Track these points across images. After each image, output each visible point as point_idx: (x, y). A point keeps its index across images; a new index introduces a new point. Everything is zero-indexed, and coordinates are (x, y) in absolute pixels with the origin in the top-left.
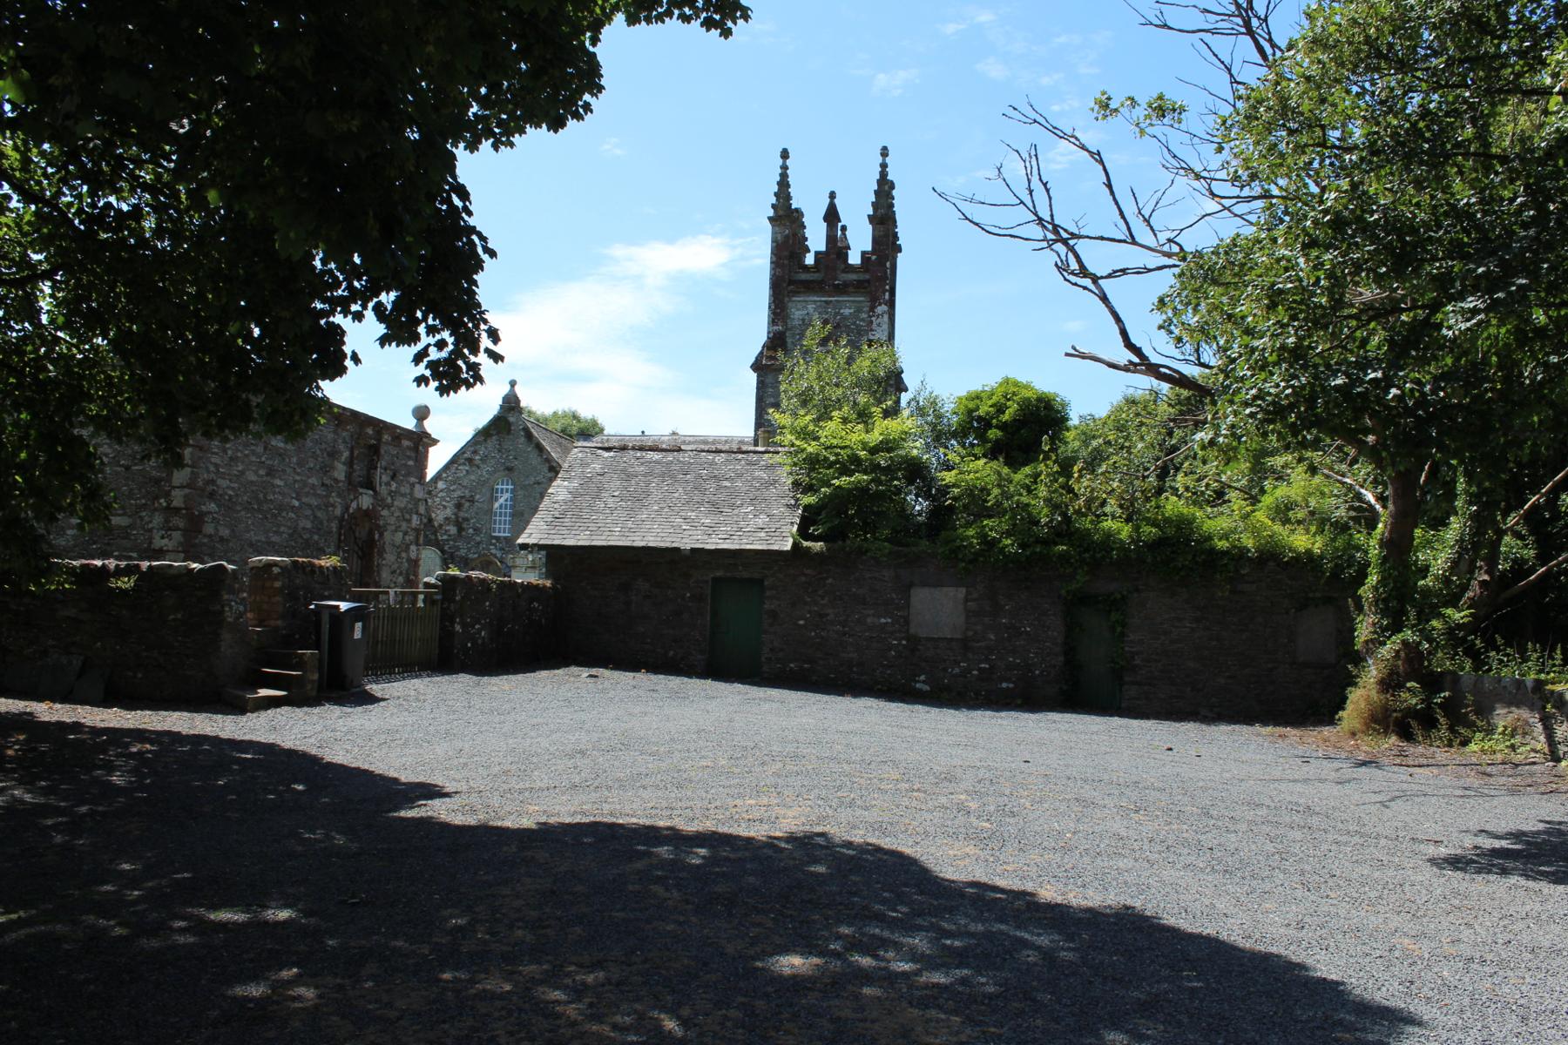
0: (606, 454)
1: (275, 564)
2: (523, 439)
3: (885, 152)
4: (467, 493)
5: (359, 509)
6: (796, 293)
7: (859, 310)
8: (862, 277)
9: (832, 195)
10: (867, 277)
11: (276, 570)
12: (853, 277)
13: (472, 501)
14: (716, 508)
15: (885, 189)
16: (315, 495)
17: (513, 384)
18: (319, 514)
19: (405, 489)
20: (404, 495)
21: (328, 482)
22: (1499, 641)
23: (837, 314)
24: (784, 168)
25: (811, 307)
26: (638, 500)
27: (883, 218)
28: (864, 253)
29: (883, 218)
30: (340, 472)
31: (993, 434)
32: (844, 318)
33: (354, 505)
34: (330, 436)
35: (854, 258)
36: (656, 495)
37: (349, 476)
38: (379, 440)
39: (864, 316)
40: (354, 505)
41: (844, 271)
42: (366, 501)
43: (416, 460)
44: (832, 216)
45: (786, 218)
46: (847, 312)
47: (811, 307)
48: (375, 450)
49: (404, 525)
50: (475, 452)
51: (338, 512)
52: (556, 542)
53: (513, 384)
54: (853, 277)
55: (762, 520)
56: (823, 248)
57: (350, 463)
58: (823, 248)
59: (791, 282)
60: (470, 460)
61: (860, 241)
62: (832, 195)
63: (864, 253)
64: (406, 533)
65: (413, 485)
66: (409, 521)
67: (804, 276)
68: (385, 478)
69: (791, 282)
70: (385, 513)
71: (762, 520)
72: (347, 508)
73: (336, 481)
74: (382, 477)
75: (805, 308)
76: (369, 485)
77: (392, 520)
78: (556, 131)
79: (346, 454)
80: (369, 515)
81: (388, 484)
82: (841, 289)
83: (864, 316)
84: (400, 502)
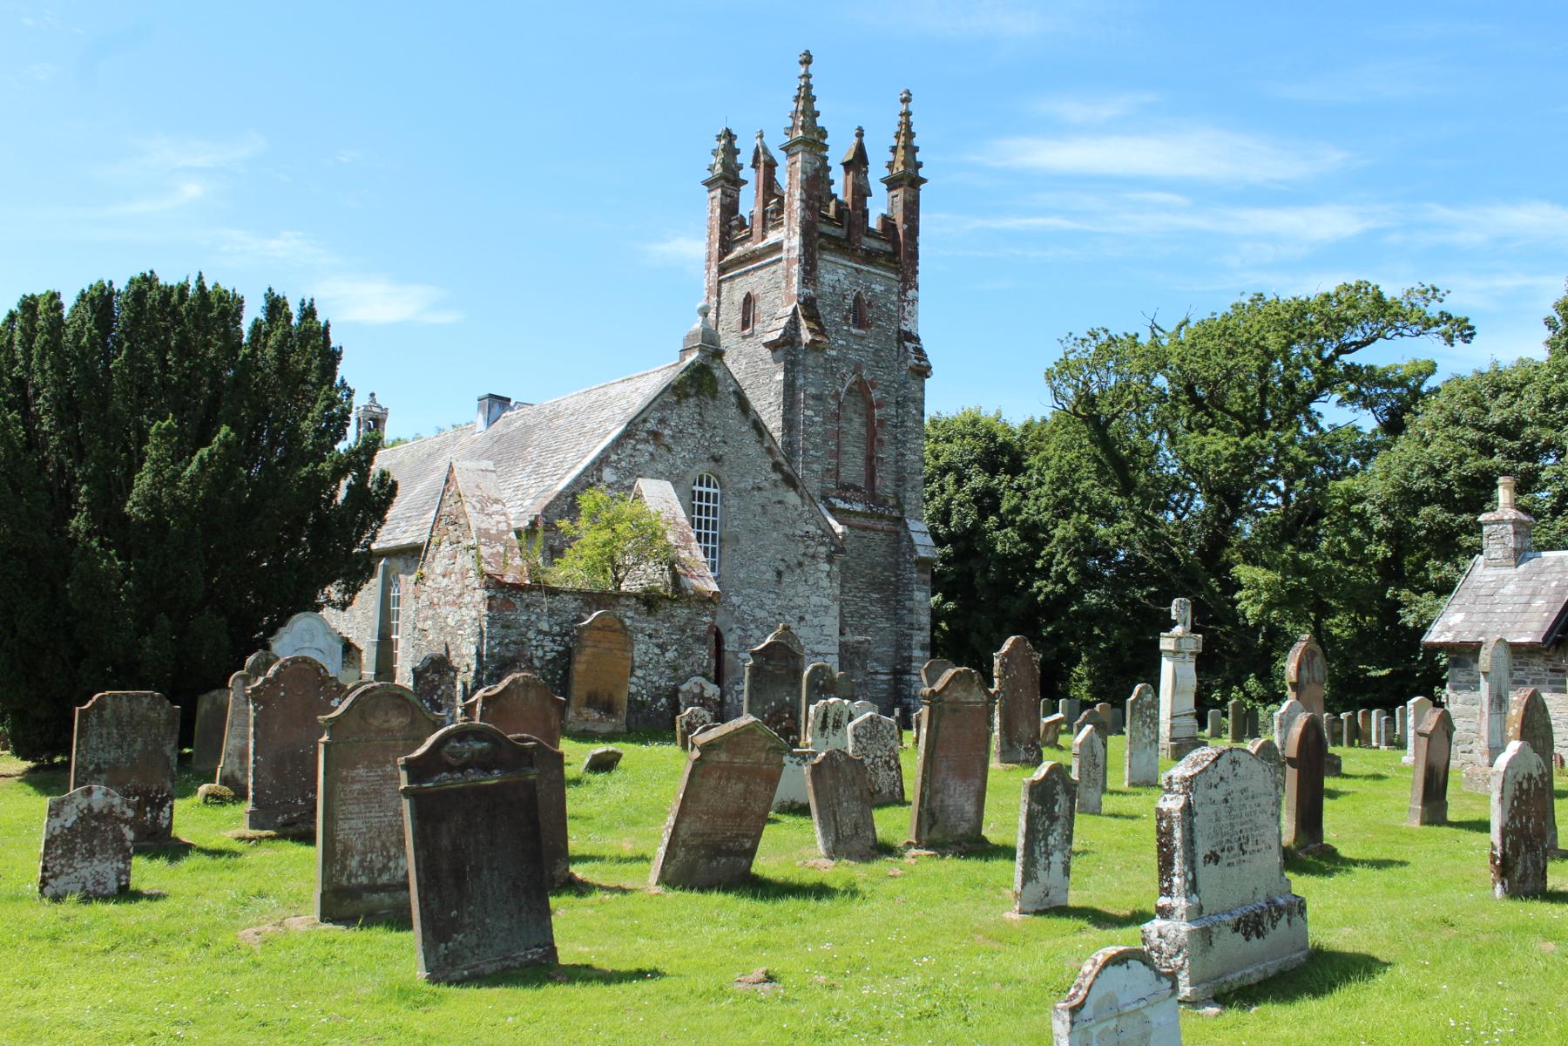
2: (733, 411)
6: (822, 248)
7: (888, 290)
9: (860, 134)
23: (868, 289)
27: (908, 181)
32: (875, 295)
39: (894, 298)
46: (878, 288)
59: (822, 235)
60: (656, 435)
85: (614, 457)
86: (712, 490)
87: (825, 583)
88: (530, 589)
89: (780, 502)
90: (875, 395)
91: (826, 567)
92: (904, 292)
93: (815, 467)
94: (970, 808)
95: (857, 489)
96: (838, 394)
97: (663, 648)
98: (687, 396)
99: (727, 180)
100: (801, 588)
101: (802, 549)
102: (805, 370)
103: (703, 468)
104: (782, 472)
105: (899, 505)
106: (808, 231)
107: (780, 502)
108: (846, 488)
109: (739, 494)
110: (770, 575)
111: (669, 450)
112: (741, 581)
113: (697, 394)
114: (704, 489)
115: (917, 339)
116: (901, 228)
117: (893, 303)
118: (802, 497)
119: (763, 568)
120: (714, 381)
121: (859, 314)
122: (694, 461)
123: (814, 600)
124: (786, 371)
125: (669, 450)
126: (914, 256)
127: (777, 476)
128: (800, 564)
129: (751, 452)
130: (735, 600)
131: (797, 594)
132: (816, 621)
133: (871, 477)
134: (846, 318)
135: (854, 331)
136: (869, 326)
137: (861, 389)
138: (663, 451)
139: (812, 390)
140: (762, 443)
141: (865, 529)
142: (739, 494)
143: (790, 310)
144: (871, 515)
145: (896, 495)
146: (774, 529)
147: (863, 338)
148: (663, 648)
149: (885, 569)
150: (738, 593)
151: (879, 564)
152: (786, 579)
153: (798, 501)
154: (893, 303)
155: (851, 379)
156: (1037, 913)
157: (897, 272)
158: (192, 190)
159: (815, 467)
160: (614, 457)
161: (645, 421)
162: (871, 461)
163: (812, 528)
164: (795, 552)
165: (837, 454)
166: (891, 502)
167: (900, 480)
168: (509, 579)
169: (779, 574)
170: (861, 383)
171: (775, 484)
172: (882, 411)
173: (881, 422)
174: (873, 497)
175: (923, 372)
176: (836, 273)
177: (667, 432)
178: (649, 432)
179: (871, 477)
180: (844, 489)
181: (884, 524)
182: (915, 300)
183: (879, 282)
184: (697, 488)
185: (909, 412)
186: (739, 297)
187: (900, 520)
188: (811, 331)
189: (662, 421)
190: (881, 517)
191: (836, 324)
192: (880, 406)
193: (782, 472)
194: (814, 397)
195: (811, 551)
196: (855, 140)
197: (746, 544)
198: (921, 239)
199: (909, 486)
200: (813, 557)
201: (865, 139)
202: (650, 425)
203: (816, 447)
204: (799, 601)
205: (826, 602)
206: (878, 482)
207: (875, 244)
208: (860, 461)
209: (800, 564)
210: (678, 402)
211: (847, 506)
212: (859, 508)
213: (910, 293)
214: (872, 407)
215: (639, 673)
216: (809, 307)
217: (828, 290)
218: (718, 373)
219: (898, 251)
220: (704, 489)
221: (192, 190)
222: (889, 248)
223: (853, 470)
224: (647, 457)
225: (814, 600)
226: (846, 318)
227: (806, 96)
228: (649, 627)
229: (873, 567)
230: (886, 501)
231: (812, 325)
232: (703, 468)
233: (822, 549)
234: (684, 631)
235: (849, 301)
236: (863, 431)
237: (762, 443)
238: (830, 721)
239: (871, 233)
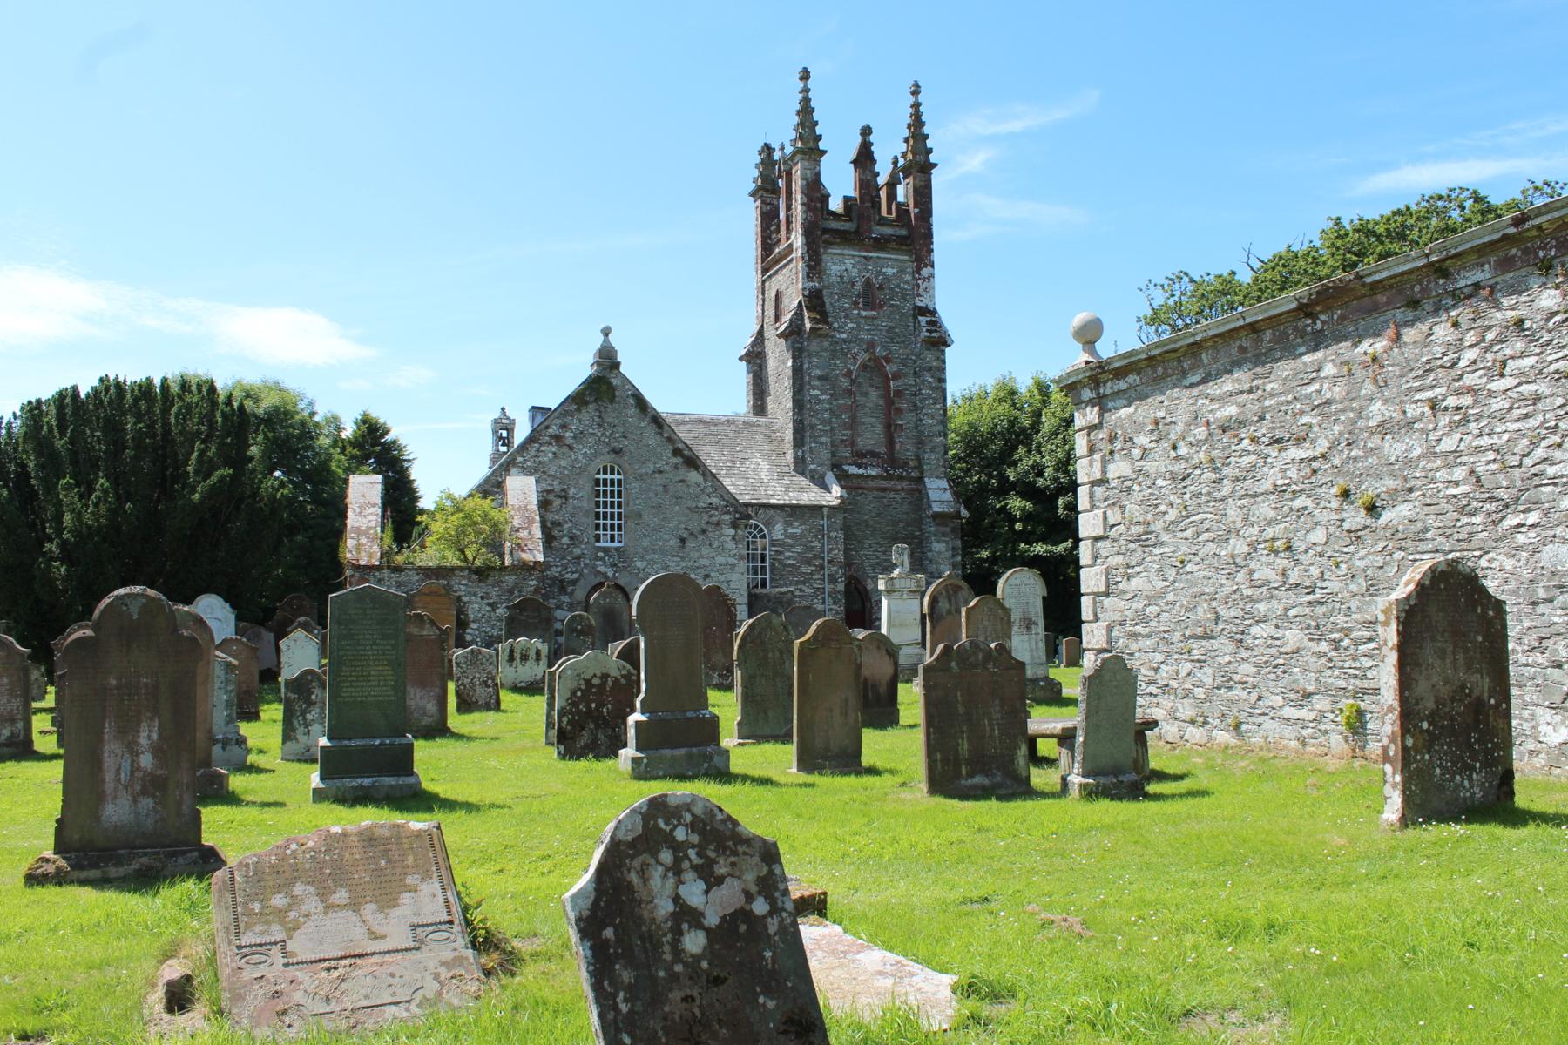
2: (632, 411)
3: (805, 75)
4: (557, 486)
6: (828, 244)
7: (902, 271)
9: (866, 131)
13: (564, 496)
16: (1392, 469)
17: (606, 332)
22: (623, 681)
23: (879, 273)
25: (849, 262)
27: (919, 164)
28: (847, 199)
32: (887, 278)
35: (836, 204)
39: (908, 278)
44: (864, 159)
46: (889, 271)
50: (564, 426)
53: (606, 332)
56: (852, 192)
58: (852, 192)
59: (826, 231)
60: (558, 439)
62: (866, 131)
63: (847, 199)
82: (881, 244)
83: (908, 278)
85: (520, 459)
86: (616, 477)
87: (731, 545)
88: (379, 568)
90: (890, 369)
91: (732, 532)
92: (918, 270)
93: (824, 439)
94: (432, 707)
95: (874, 455)
96: (849, 372)
97: (494, 606)
98: (586, 403)
99: (766, 190)
100: (705, 551)
101: (706, 517)
102: (810, 356)
103: (606, 460)
104: (682, 456)
105: (919, 467)
106: (809, 232)
108: (862, 455)
109: (640, 478)
110: (674, 542)
111: (571, 448)
112: (645, 549)
113: (596, 401)
114: (609, 477)
115: (933, 312)
116: (913, 211)
117: (907, 282)
120: (611, 389)
121: (870, 296)
122: (595, 455)
123: (720, 560)
124: (794, 358)
125: (571, 448)
126: (929, 236)
127: (678, 460)
128: (704, 531)
129: (652, 442)
130: (639, 564)
131: (702, 557)
133: (891, 443)
134: (856, 303)
135: (864, 313)
136: (881, 307)
137: (875, 367)
138: (565, 450)
139: (818, 372)
141: (884, 490)
142: (640, 478)
143: (796, 303)
144: (890, 477)
145: (918, 458)
146: (676, 504)
147: (874, 318)
148: (494, 606)
149: (908, 525)
150: (642, 558)
151: (901, 521)
152: (690, 544)
153: (700, 479)
154: (907, 282)
155: (863, 357)
156: (299, 761)
157: (909, 253)
159: (824, 439)
160: (520, 459)
161: (547, 428)
162: (890, 429)
163: (715, 501)
164: (696, 523)
165: (853, 425)
166: (912, 464)
167: (920, 443)
168: (362, 563)
169: (683, 540)
170: (876, 359)
172: (899, 382)
173: (898, 393)
174: (892, 460)
175: (940, 342)
176: (843, 264)
177: (568, 434)
178: (551, 436)
179: (891, 443)
180: (860, 457)
181: (905, 484)
182: (932, 276)
183: (891, 265)
184: (601, 477)
185: (924, 381)
186: (773, 294)
187: (920, 479)
188: (812, 320)
189: (564, 426)
190: (900, 478)
191: (846, 309)
192: (896, 377)
193: (682, 456)
194: (819, 378)
195: (715, 519)
196: (859, 139)
197: (649, 518)
198: (936, 220)
199: (928, 448)
200: (717, 524)
201: (872, 138)
202: (553, 430)
203: (823, 422)
204: (703, 562)
205: (732, 561)
206: (898, 447)
207: (888, 231)
208: (879, 429)
209: (704, 531)
210: (578, 410)
211: (861, 471)
212: (873, 472)
213: (925, 272)
214: (888, 379)
215: (474, 626)
216: (814, 301)
217: (834, 280)
218: (615, 382)
219: (913, 236)
220: (609, 477)
222: (904, 232)
223: (871, 436)
224: (551, 456)
225: (720, 560)
226: (856, 303)
227: (806, 110)
228: (481, 591)
229: (895, 524)
230: (906, 463)
231: (813, 315)
232: (606, 460)
233: (727, 517)
234: (511, 593)
235: (858, 287)
236: (881, 402)
238: (517, 655)
239: (883, 222)
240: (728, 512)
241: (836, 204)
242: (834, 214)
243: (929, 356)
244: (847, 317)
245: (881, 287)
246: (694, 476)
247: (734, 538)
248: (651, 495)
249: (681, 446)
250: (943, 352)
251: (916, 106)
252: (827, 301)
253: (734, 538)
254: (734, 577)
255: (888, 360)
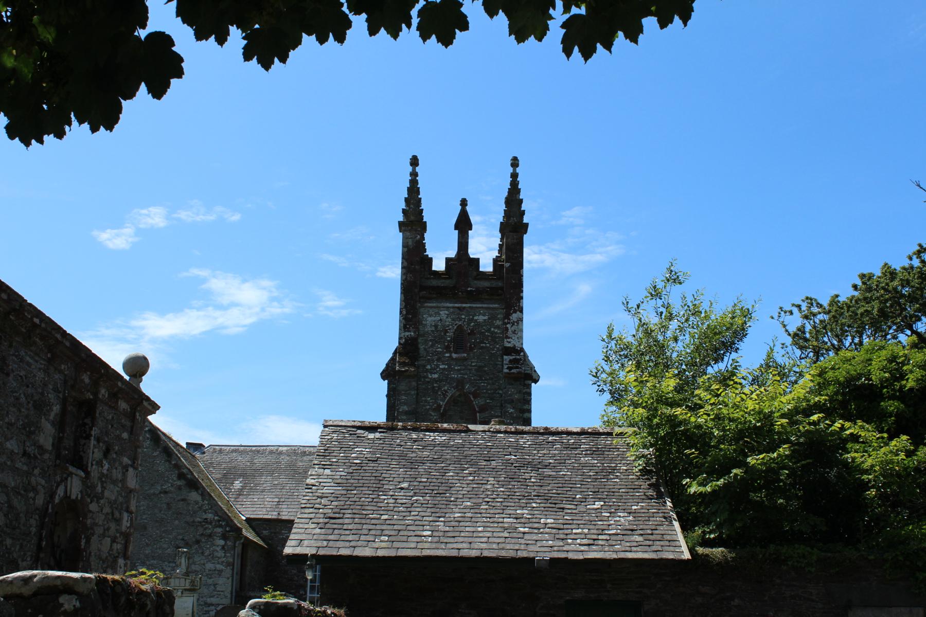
0: (371, 436)
1: (67, 587)
5: (67, 497)
6: (429, 299)
7: (493, 318)
8: (495, 284)
9: (464, 203)
10: (500, 284)
11: (68, 603)
12: (486, 284)
14: (553, 505)
15: (513, 201)
18: (15, 502)
19: (117, 474)
20: (114, 482)
21: (31, 450)
23: (472, 320)
24: (414, 174)
25: (443, 313)
26: (439, 496)
27: (514, 228)
28: (448, 260)
29: (514, 228)
30: (46, 437)
31: (892, 406)
32: (478, 324)
33: (60, 492)
34: (41, 375)
36: (460, 488)
37: (58, 443)
38: (96, 394)
40: (60, 492)
41: (476, 279)
42: (75, 488)
43: (131, 433)
45: (413, 223)
46: (481, 318)
47: (443, 313)
48: (88, 409)
49: (113, 526)
51: (40, 500)
52: (344, 552)
54: (486, 284)
55: (624, 519)
57: (60, 424)
59: (423, 288)
61: (485, 248)
62: (464, 203)
64: (114, 541)
65: (126, 468)
66: (118, 521)
67: (435, 283)
68: (98, 455)
69: (423, 288)
70: (93, 507)
71: (624, 519)
72: (52, 495)
73: (40, 447)
74: (94, 452)
75: (438, 315)
76: (79, 462)
77: (100, 519)
78: (266, 64)
79: (56, 409)
80: (74, 508)
81: (100, 463)
82: (475, 296)
83: (498, 323)
84: (111, 493)
87: (221, 554)
89: (183, 500)
91: (222, 542)
92: (507, 316)
96: (439, 406)
101: (201, 530)
107: (183, 500)
117: (498, 327)
118: (202, 495)
119: (165, 546)
121: (460, 341)
123: (209, 566)
128: (198, 542)
129: (161, 469)
132: (210, 581)
135: (454, 356)
136: (471, 349)
139: (406, 408)
140: (170, 462)
147: (465, 359)
153: (199, 498)
154: (498, 327)
158: (585, 289)
163: (210, 516)
171: (180, 488)
175: (531, 377)
191: (439, 353)
194: (406, 413)
195: (209, 531)
200: (210, 536)
201: (468, 208)
205: (219, 567)
209: (198, 542)
213: (514, 317)
217: (429, 329)
221: (585, 289)
225: (209, 566)
233: (219, 530)
237: (170, 462)
240: (221, 526)
241: (439, 265)
242: (484, 274)
243: (513, 391)
244: (438, 360)
245: (472, 333)
246: (194, 496)
247: (223, 548)
248: (156, 511)
249: (185, 471)
250: (529, 387)
251: (514, 176)
252: (422, 347)
253: (223, 548)
254: (221, 581)
255: (476, 396)
